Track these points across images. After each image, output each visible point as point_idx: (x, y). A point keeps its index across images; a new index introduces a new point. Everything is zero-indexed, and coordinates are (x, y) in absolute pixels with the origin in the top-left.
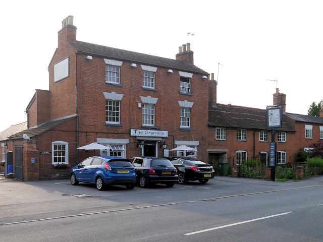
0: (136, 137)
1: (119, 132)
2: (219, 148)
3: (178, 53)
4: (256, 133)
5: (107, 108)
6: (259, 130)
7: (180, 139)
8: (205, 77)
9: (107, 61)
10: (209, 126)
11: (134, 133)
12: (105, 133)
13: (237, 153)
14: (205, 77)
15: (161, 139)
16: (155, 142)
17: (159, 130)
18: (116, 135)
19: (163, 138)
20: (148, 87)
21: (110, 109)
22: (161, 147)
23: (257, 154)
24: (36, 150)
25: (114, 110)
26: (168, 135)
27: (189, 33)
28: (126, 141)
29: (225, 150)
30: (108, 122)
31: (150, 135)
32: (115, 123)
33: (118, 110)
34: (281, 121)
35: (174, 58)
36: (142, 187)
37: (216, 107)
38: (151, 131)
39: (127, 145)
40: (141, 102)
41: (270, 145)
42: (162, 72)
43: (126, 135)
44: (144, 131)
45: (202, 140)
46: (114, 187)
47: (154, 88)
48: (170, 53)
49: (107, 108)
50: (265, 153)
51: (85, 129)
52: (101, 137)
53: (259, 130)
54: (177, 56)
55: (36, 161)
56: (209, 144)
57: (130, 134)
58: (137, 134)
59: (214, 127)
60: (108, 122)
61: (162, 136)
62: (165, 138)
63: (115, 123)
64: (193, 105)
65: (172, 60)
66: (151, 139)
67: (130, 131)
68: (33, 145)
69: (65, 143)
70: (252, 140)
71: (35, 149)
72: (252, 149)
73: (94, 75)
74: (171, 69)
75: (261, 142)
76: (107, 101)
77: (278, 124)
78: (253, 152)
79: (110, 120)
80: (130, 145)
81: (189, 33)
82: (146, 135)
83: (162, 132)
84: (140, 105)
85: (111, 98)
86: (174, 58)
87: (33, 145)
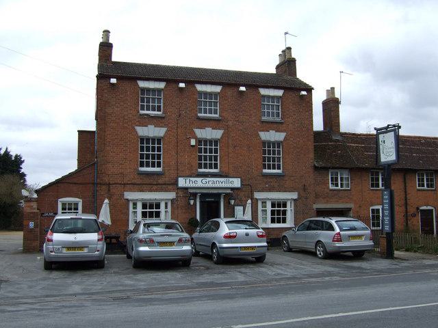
0: (186, 188)
1: (160, 181)
2: (337, 202)
3: (278, 63)
4: (408, 177)
5: (264, 152)
6: (414, 171)
7: (263, 190)
8: (304, 93)
9: (263, 92)
10: (316, 168)
11: (182, 182)
12: (138, 184)
13: (373, 210)
14: (304, 93)
15: (229, 191)
16: (218, 195)
17: (226, 177)
18: (155, 187)
19: (232, 189)
20: (208, 115)
21: (211, 152)
22: (227, 204)
23: (412, 210)
24: (36, 211)
25: (153, 150)
26: (241, 185)
27: (286, 33)
28: (171, 195)
29: (348, 206)
30: (266, 171)
31: (210, 185)
32: (156, 169)
33: (216, 152)
34: (398, 151)
35: (274, 71)
36: (320, 258)
37: (339, 138)
38: (212, 179)
39: (172, 201)
40: (196, 138)
41: (383, 197)
42: (229, 92)
43: (170, 187)
44: (199, 180)
45: (303, 190)
46: (345, 256)
47: (217, 116)
48: (268, 65)
49: (264, 152)
50: (429, 208)
51: (106, 180)
52: (131, 190)
53: (414, 171)
54: (278, 67)
55: (36, 226)
56: (317, 196)
57: (177, 185)
58: (188, 185)
59: (326, 169)
60: (266, 171)
61: (231, 186)
62: (237, 189)
63: (156, 169)
64: (285, 137)
65: (271, 75)
66: (215, 191)
67: (177, 181)
68: (32, 204)
69: (77, 199)
70: (402, 187)
71: (35, 209)
72: (404, 202)
73: (122, 104)
74: (304, 90)
75: (419, 190)
76: (142, 140)
77: (393, 157)
78: (404, 208)
79: (269, 168)
80: (177, 200)
81: (286, 33)
82: (206, 186)
83: (231, 179)
84: (193, 142)
85: (277, 139)
86: (274, 71)
87: (32, 204)
